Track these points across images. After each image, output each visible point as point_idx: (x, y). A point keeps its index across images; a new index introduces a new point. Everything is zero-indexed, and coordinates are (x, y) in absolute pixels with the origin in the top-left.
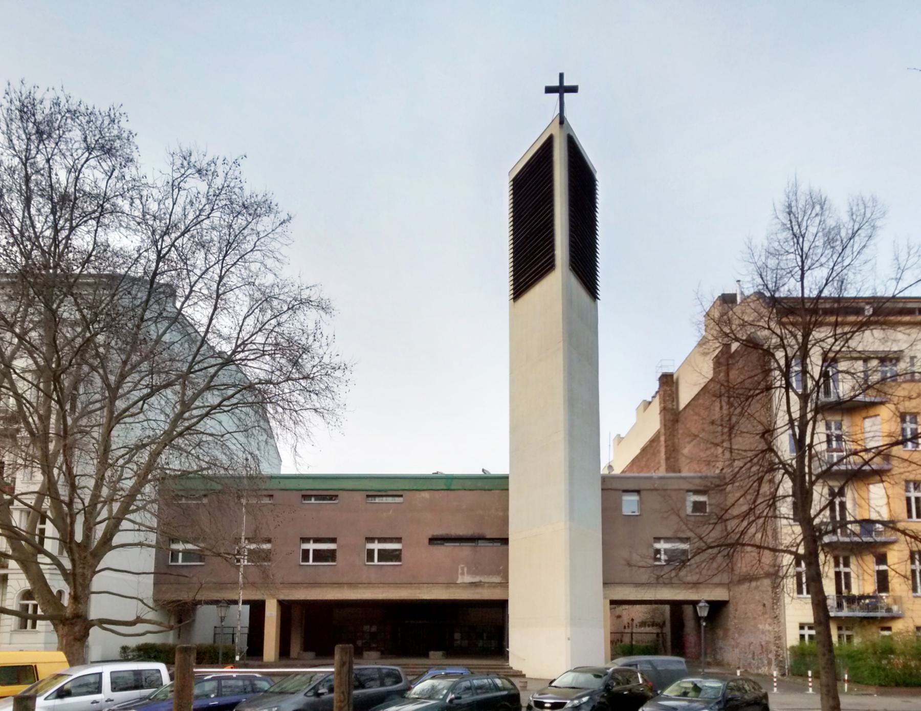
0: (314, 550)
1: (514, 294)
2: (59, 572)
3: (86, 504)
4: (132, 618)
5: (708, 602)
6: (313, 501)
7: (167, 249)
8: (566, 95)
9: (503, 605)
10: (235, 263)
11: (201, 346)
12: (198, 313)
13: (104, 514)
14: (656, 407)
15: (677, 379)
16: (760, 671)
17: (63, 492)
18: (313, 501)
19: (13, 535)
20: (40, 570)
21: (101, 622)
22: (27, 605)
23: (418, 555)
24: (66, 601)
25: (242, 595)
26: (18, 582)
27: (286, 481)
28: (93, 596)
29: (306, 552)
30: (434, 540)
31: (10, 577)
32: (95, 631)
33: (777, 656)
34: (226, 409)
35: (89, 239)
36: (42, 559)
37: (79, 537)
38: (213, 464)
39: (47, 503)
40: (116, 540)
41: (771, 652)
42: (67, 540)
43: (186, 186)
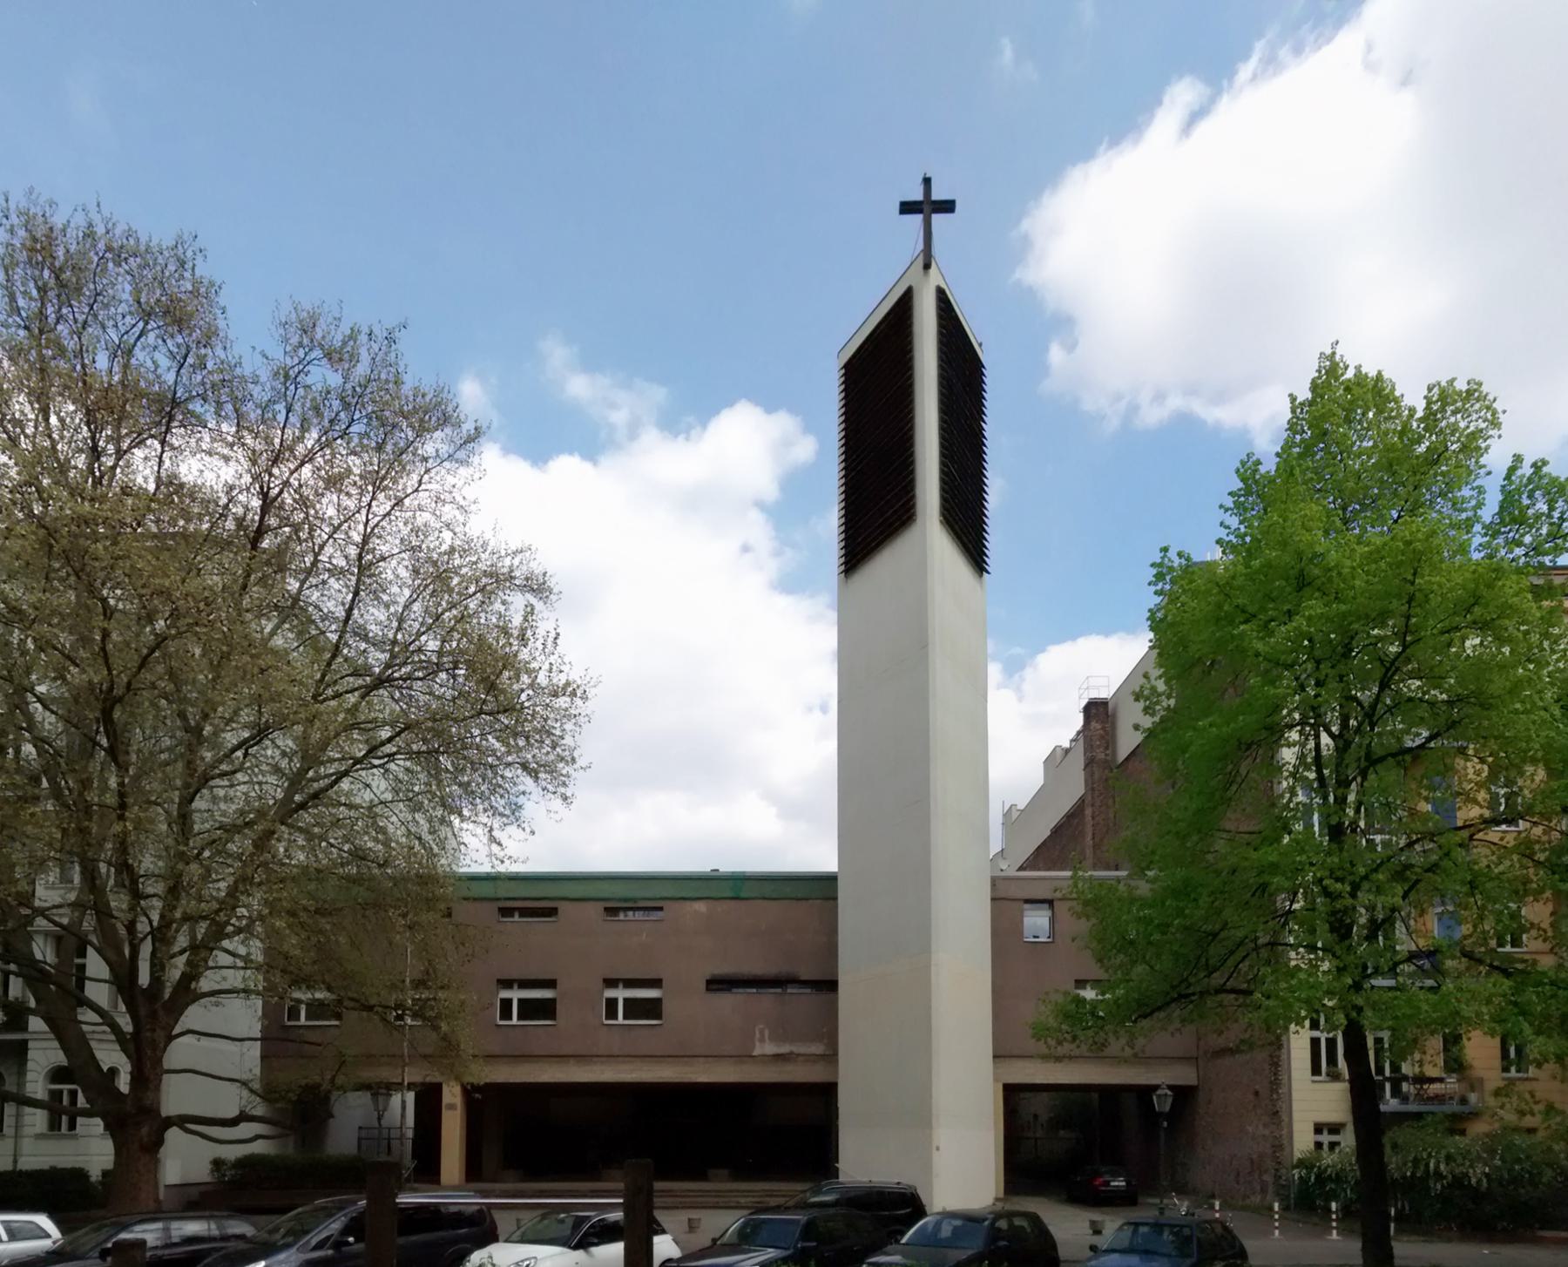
0: (625, 1000)
1: (845, 563)
2: (113, 1037)
3: (155, 924)
4: (233, 1112)
5: (1170, 1087)
6: (517, 918)
7: (277, 490)
8: (936, 218)
9: (828, 1091)
10: (389, 514)
11: (334, 656)
12: (330, 598)
13: (182, 941)
14: (1078, 760)
15: (1115, 710)
16: (1248, 1202)
17: (118, 902)
18: (517, 918)
19: (35, 975)
20: (83, 1034)
21: (182, 1121)
22: (61, 1092)
23: (688, 1008)
24: (123, 1084)
25: (413, 1075)
26: (44, 1054)
27: (474, 884)
28: (165, 1077)
29: (612, 1003)
30: (718, 984)
31: (30, 1044)
32: (173, 1134)
33: (1277, 1177)
34: (376, 762)
35: (148, 472)
36: (87, 1015)
37: (144, 979)
38: (359, 855)
39: (89, 923)
40: (205, 984)
41: (1266, 1171)
42: (123, 980)
43: (309, 380)
